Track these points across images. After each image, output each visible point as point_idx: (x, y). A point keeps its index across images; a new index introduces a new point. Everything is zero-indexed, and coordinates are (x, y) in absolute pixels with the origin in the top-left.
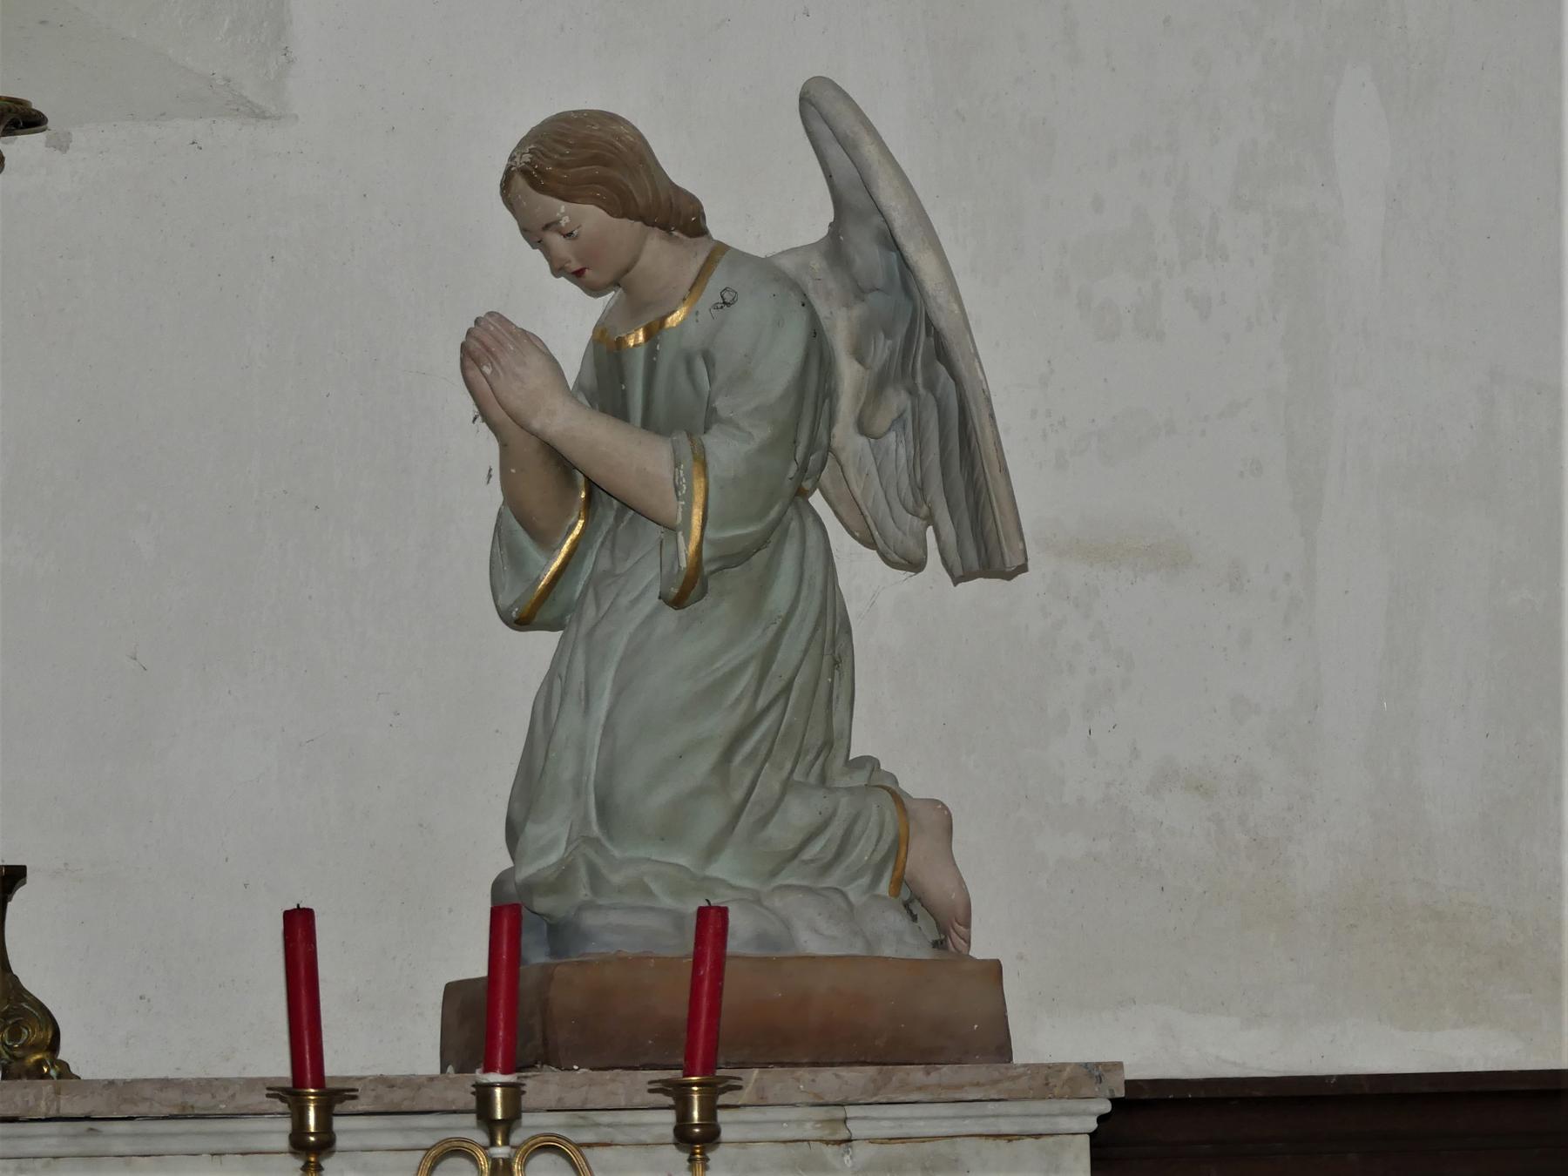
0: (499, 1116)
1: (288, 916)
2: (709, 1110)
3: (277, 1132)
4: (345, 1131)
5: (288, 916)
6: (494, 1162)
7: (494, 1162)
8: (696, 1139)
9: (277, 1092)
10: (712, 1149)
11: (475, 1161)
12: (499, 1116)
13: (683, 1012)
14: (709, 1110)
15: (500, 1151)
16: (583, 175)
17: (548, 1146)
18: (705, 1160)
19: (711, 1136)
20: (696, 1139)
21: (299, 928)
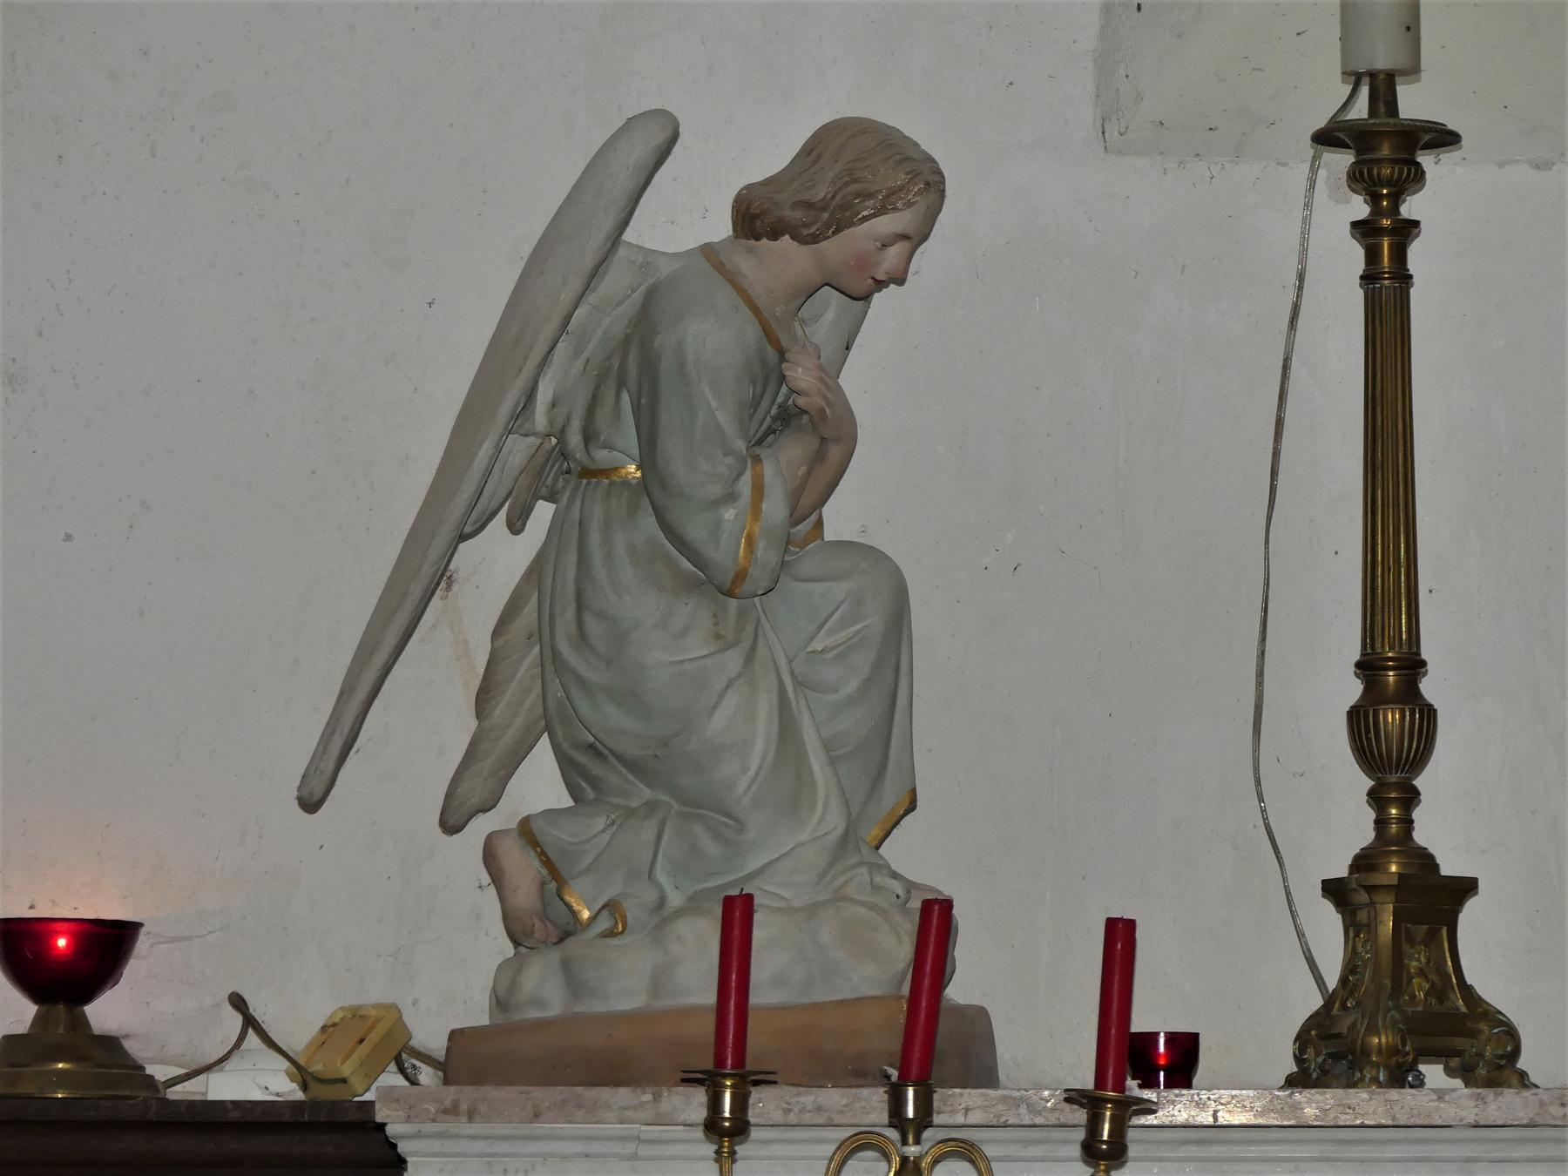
0: (911, 1114)
1: (1111, 924)
2: (740, 1104)
3: (694, 1104)
4: (1140, 1141)
5: (1111, 924)
6: (904, 1160)
7: (904, 1160)
8: (727, 1133)
9: (1074, 1097)
10: (740, 1143)
11: (889, 1162)
12: (911, 1114)
13: (711, 998)
14: (740, 1104)
15: (912, 1150)
16: (1326, 138)
17: (967, 1151)
18: (732, 1153)
19: (741, 1128)
20: (727, 1133)
21: (1120, 939)
